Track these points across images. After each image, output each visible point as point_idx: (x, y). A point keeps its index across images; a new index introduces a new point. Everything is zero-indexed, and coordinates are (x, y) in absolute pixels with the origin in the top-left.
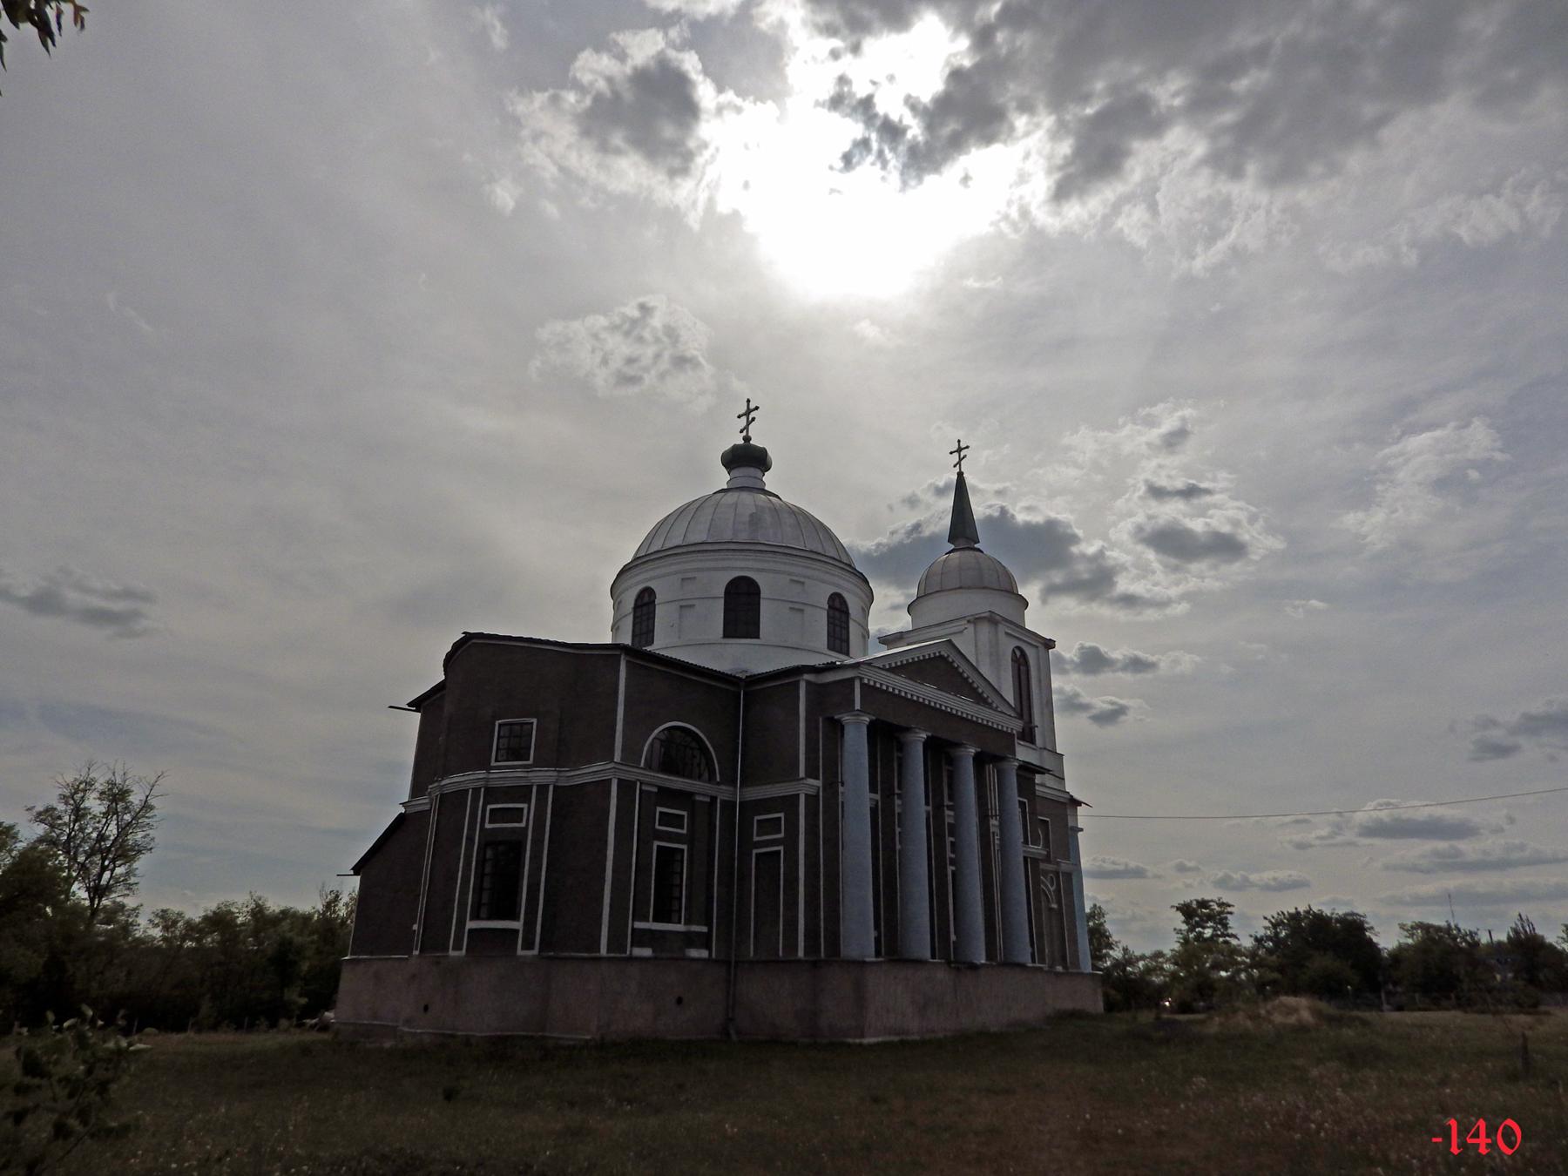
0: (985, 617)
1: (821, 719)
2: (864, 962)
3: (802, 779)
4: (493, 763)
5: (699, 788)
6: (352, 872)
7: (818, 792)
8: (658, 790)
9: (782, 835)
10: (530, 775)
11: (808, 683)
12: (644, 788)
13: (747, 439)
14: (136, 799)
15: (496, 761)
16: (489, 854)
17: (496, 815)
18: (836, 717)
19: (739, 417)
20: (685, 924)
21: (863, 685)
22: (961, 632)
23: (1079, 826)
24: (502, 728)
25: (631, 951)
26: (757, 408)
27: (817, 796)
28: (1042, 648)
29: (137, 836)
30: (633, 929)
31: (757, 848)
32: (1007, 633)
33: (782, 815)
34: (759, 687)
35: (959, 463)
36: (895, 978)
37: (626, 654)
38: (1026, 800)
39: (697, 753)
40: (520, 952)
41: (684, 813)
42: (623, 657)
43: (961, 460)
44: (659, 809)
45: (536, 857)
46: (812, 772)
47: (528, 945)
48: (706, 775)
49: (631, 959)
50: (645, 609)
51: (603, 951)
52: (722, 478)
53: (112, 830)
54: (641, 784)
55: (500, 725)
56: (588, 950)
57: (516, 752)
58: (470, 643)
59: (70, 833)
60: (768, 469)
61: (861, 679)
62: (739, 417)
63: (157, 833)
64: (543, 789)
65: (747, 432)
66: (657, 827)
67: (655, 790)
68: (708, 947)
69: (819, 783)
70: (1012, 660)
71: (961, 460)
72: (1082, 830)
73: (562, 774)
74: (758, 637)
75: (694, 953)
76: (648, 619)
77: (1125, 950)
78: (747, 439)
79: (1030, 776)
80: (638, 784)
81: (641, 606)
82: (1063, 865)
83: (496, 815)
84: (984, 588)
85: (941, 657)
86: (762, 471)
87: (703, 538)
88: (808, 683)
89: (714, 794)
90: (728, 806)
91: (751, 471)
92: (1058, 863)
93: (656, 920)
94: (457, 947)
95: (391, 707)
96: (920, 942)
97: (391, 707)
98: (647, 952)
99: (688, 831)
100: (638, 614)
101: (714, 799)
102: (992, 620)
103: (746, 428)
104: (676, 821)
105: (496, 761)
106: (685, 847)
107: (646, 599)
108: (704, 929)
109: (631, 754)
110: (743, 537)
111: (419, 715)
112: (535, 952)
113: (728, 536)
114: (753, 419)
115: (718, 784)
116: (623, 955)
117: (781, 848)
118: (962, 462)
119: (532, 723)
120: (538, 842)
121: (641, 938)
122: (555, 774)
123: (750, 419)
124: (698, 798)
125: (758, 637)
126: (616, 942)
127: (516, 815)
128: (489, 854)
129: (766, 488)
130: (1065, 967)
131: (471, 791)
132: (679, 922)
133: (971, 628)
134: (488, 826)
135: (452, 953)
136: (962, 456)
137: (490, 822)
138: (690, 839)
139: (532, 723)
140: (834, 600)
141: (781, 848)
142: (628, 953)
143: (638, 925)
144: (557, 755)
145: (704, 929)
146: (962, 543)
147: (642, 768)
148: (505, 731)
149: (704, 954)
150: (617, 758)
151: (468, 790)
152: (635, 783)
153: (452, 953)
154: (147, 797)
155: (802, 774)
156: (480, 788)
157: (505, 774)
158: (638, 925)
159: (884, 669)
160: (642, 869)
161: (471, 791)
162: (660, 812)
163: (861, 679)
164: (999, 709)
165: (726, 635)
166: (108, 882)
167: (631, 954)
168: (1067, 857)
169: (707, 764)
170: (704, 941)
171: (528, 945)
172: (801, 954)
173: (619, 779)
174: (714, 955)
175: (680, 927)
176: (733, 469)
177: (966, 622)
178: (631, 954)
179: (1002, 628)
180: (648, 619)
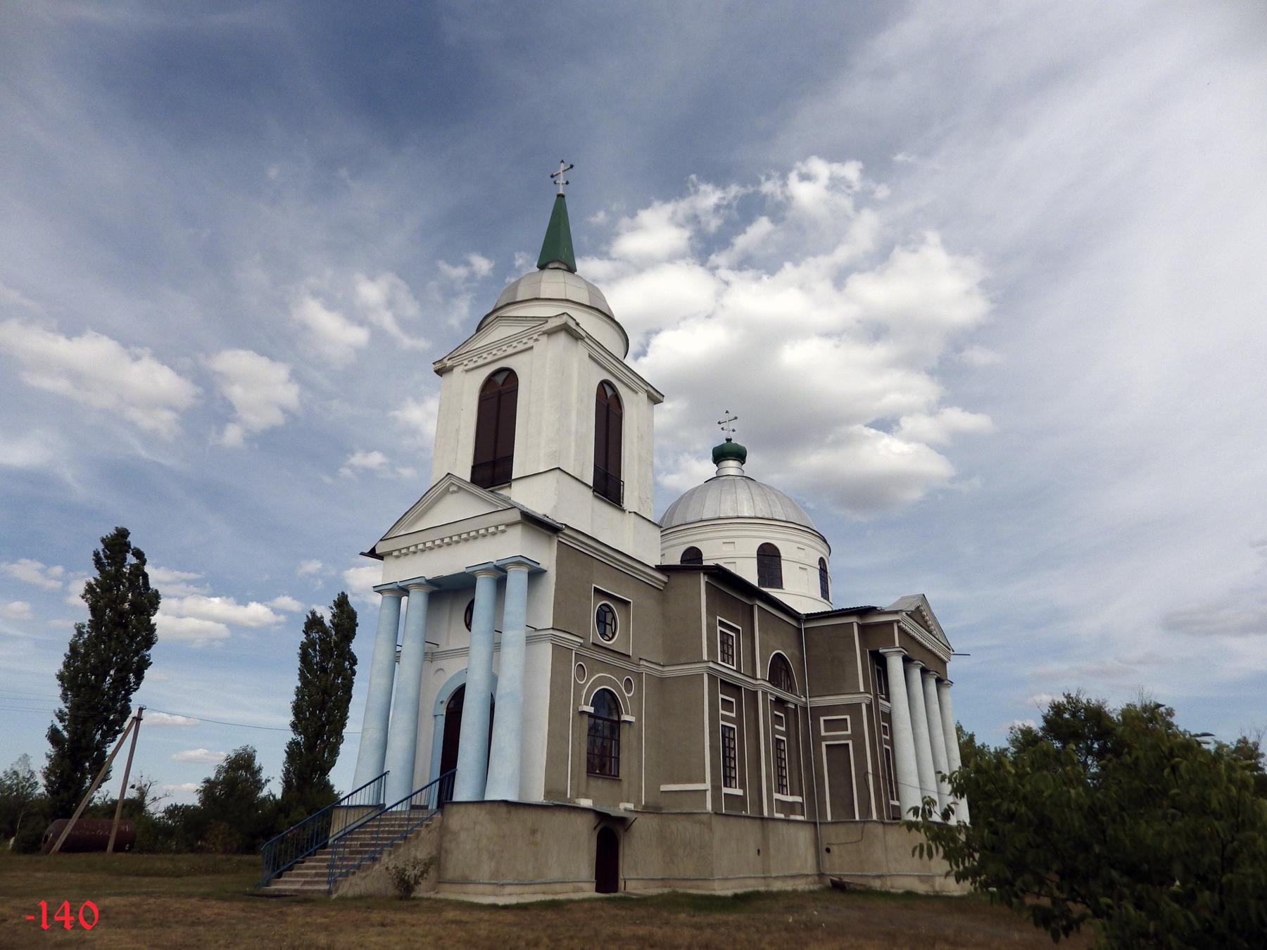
93: (792, 794)
175: (790, 799)
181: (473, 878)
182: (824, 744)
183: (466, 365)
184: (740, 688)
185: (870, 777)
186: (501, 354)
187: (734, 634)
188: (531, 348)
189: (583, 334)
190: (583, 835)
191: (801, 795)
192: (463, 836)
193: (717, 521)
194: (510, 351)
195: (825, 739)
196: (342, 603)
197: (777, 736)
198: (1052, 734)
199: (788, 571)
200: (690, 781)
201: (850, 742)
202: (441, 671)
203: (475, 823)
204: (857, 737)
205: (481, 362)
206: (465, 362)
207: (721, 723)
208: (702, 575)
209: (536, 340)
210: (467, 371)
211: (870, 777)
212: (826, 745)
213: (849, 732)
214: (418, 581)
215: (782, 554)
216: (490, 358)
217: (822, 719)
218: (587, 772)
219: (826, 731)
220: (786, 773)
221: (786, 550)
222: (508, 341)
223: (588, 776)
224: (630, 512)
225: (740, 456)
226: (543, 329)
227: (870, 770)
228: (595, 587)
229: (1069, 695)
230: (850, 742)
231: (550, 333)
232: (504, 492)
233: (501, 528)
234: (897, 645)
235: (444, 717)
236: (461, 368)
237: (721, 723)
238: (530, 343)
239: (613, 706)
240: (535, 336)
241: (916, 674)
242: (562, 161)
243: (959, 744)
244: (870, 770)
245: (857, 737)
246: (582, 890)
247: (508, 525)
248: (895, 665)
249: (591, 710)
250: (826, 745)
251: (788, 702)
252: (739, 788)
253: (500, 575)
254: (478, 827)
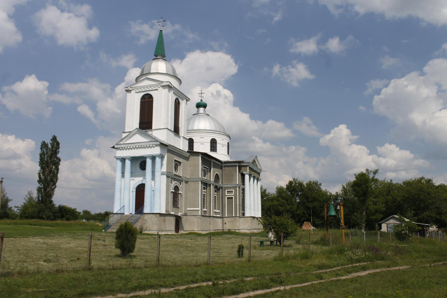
93: (217, 210)
179: (172, 92)
181: (152, 229)
182: (226, 197)
183: (136, 91)
184: (207, 184)
185: (238, 206)
186: (147, 89)
187: (206, 169)
188: (157, 90)
189: (172, 86)
190: (173, 219)
191: (220, 210)
192: (148, 221)
193: (198, 131)
194: (151, 89)
195: (227, 196)
196: (54, 139)
197: (215, 195)
198: (288, 190)
199: (219, 147)
200: (195, 207)
201: (233, 197)
202: (133, 180)
203: (152, 218)
204: (235, 195)
205: (141, 90)
206: (136, 90)
207: (203, 193)
208: (200, 154)
209: (159, 87)
210: (137, 92)
211: (238, 206)
212: (227, 198)
213: (233, 194)
214: (129, 157)
215: (217, 142)
216: (144, 90)
217: (226, 190)
218: (173, 206)
219: (227, 193)
220: (216, 205)
221: (219, 140)
222: (150, 86)
223: (173, 207)
225: (205, 106)
226: (162, 85)
227: (238, 204)
228: (175, 160)
229: (294, 178)
230: (233, 197)
231: (164, 87)
232: (150, 133)
233: (154, 146)
234: (248, 171)
235: (135, 192)
236: (134, 91)
237: (203, 193)
238: (157, 88)
239: (177, 189)
240: (159, 86)
241: (252, 179)
242: (162, 18)
243: (261, 192)
244: (238, 204)
245: (235, 195)
246: (173, 232)
247: (156, 145)
248: (247, 177)
249: (174, 191)
250: (227, 198)
251: (218, 186)
253: (153, 158)
254: (152, 219)
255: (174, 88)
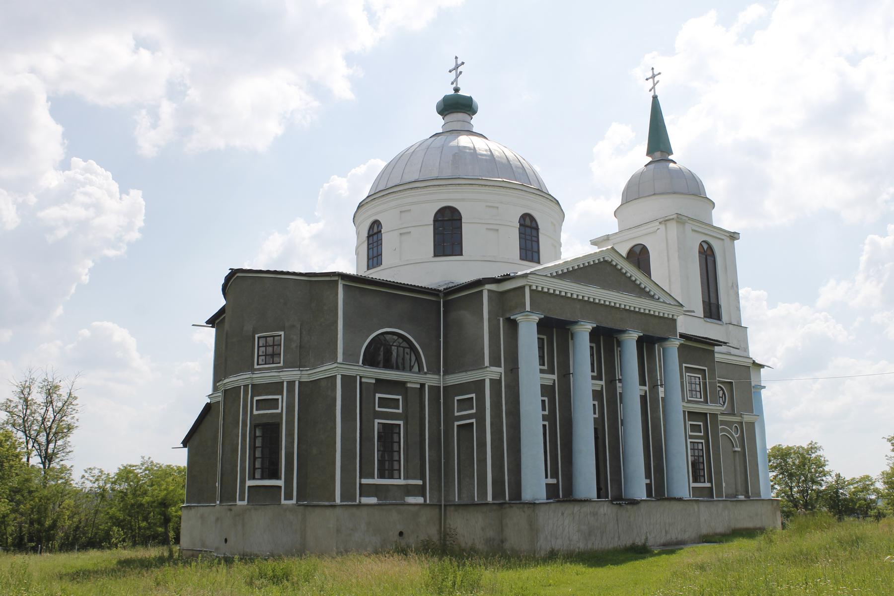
0: (673, 219)
1: (501, 319)
2: (535, 503)
3: (487, 367)
4: (256, 367)
5: (412, 378)
6: (182, 446)
7: (501, 377)
8: (376, 381)
9: (474, 411)
10: (281, 374)
11: (489, 291)
12: (363, 380)
13: (457, 90)
14: (63, 392)
15: (258, 364)
16: (258, 433)
17: (261, 404)
18: (512, 318)
19: (450, 71)
20: (404, 479)
21: (532, 291)
22: (655, 232)
23: (762, 385)
24: (260, 339)
25: (360, 500)
26: (463, 63)
27: (500, 381)
28: (727, 240)
29: (67, 419)
30: (360, 484)
31: (701, 436)
32: (693, 230)
33: (473, 395)
34: (451, 298)
35: (653, 88)
36: (563, 514)
37: (342, 279)
38: (706, 368)
39: (408, 350)
40: (283, 502)
41: (701, 423)
42: (340, 281)
43: (655, 85)
44: (378, 395)
45: (290, 434)
46: (495, 362)
47: (289, 497)
48: (416, 368)
49: (360, 505)
50: (375, 237)
51: (338, 501)
52: (437, 123)
53: (50, 414)
54: (361, 377)
55: (259, 338)
56: (328, 500)
57: (272, 357)
58: (236, 276)
59: (24, 417)
60: (474, 112)
61: (530, 286)
62: (450, 71)
63: (79, 416)
64: (291, 384)
65: (457, 84)
66: (377, 409)
67: (374, 381)
68: (423, 495)
69: (501, 370)
70: (700, 252)
71: (655, 85)
72: (764, 387)
73: (304, 373)
74: (461, 254)
75: (411, 500)
76: (377, 246)
77: (838, 476)
78: (457, 90)
79: (710, 348)
80: (358, 378)
81: (372, 235)
82: (745, 416)
83: (261, 404)
84: (675, 193)
85: (606, 261)
86: (469, 115)
87: (415, 177)
88: (489, 291)
89: (422, 381)
90: (435, 390)
91: (460, 116)
92: (741, 415)
93: (381, 476)
94: (242, 499)
95: (193, 325)
96: (638, 487)
97: (193, 325)
98: (373, 500)
99: (403, 411)
100: (371, 242)
101: (423, 385)
102: (680, 219)
103: (456, 80)
104: (394, 403)
105: (258, 364)
106: (401, 423)
107: (375, 230)
108: (420, 482)
109: (350, 357)
110: (447, 173)
111: (214, 330)
112: (294, 501)
113: (435, 174)
114: (461, 73)
115: (426, 373)
116: (354, 503)
117: (474, 421)
118: (652, 85)
119: (281, 335)
120: (290, 423)
121: (366, 490)
122: (299, 372)
123: (458, 73)
124: (409, 385)
125: (461, 254)
126: (347, 494)
127: (274, 403)
128: (258, 433)
129: (474, 130)
130: (747, 496)
131: (242, 387)
132: (400, 478)
133: (662, 227)
134: (255, 412)
135: (239, 503)
136: (655, 82)
137: (257, 410)
138: (405, 417)
139: (281, 335)
140: (524, 220)
141: (474, 421)
142: (358, 501)
143: (364, 481)
144: (298, 361)
145: (420, 482)
146: (658, 155)
147: (360, 366)
148: (262, 342)
149: (420, 500)
150: (340, 359)
151: (240, 386)
152: (356, 377)
153: (239, 503)
154: (71, 390)
155: (487, 363)
156: (248, 385)
157: (264, 375)
158: (364, 481)
159: (552, 276)
160: (366, 438)
161: (242, 387)
162: (379, 398)
163: (530, 286)
164: (661, 300)
165: (435, 255)
166: (54, 451)
167: (360, 502)
168: (751, 410)
169: (416, 359)
170: (420, 491)
171: (289, 497)
172: (490, 498)
173: (341, 375)
174: (428, 502)
175: (401, 482)
176: (445, 115)
177: (658, 223)
178: (360, 502)
179: (688, 227)
180: (377, 246)
184: (706, 414)
224: (726, 324)
252: (708, 482)
255: (689, 222)
